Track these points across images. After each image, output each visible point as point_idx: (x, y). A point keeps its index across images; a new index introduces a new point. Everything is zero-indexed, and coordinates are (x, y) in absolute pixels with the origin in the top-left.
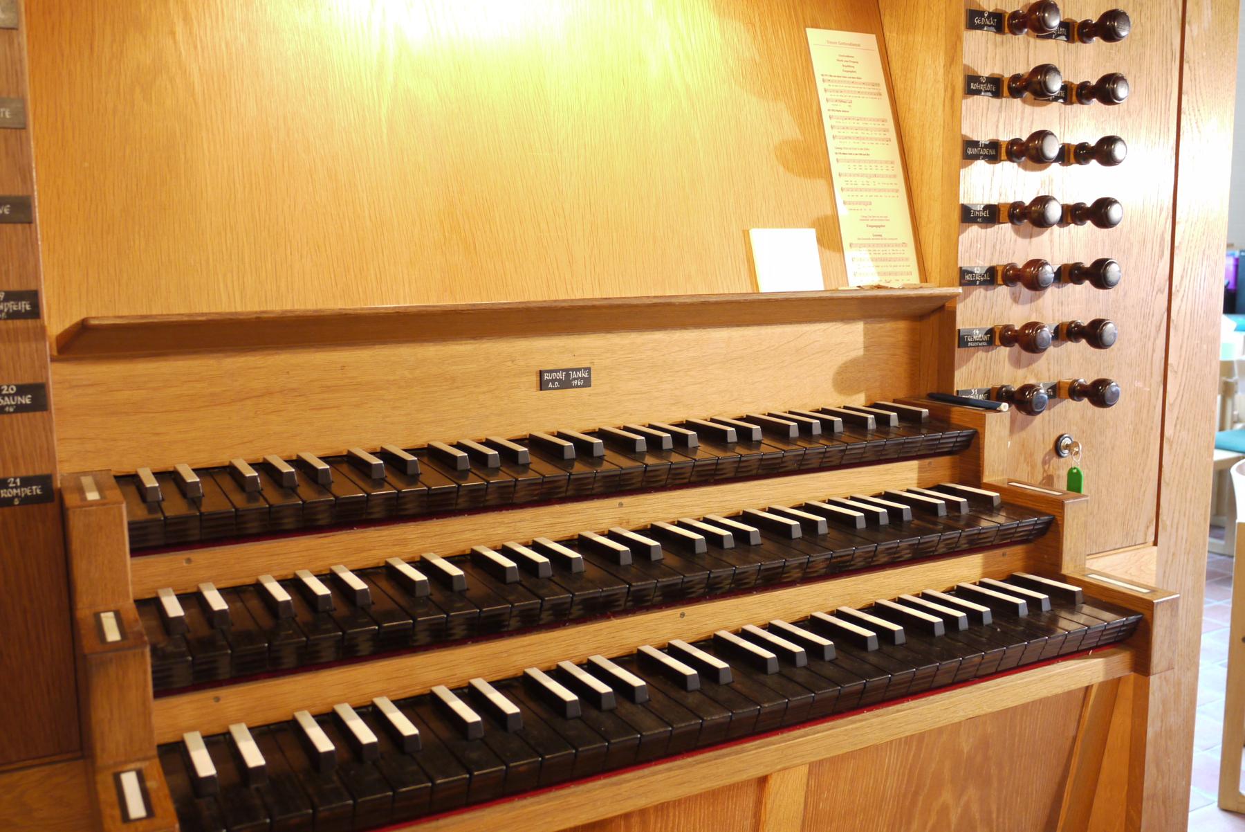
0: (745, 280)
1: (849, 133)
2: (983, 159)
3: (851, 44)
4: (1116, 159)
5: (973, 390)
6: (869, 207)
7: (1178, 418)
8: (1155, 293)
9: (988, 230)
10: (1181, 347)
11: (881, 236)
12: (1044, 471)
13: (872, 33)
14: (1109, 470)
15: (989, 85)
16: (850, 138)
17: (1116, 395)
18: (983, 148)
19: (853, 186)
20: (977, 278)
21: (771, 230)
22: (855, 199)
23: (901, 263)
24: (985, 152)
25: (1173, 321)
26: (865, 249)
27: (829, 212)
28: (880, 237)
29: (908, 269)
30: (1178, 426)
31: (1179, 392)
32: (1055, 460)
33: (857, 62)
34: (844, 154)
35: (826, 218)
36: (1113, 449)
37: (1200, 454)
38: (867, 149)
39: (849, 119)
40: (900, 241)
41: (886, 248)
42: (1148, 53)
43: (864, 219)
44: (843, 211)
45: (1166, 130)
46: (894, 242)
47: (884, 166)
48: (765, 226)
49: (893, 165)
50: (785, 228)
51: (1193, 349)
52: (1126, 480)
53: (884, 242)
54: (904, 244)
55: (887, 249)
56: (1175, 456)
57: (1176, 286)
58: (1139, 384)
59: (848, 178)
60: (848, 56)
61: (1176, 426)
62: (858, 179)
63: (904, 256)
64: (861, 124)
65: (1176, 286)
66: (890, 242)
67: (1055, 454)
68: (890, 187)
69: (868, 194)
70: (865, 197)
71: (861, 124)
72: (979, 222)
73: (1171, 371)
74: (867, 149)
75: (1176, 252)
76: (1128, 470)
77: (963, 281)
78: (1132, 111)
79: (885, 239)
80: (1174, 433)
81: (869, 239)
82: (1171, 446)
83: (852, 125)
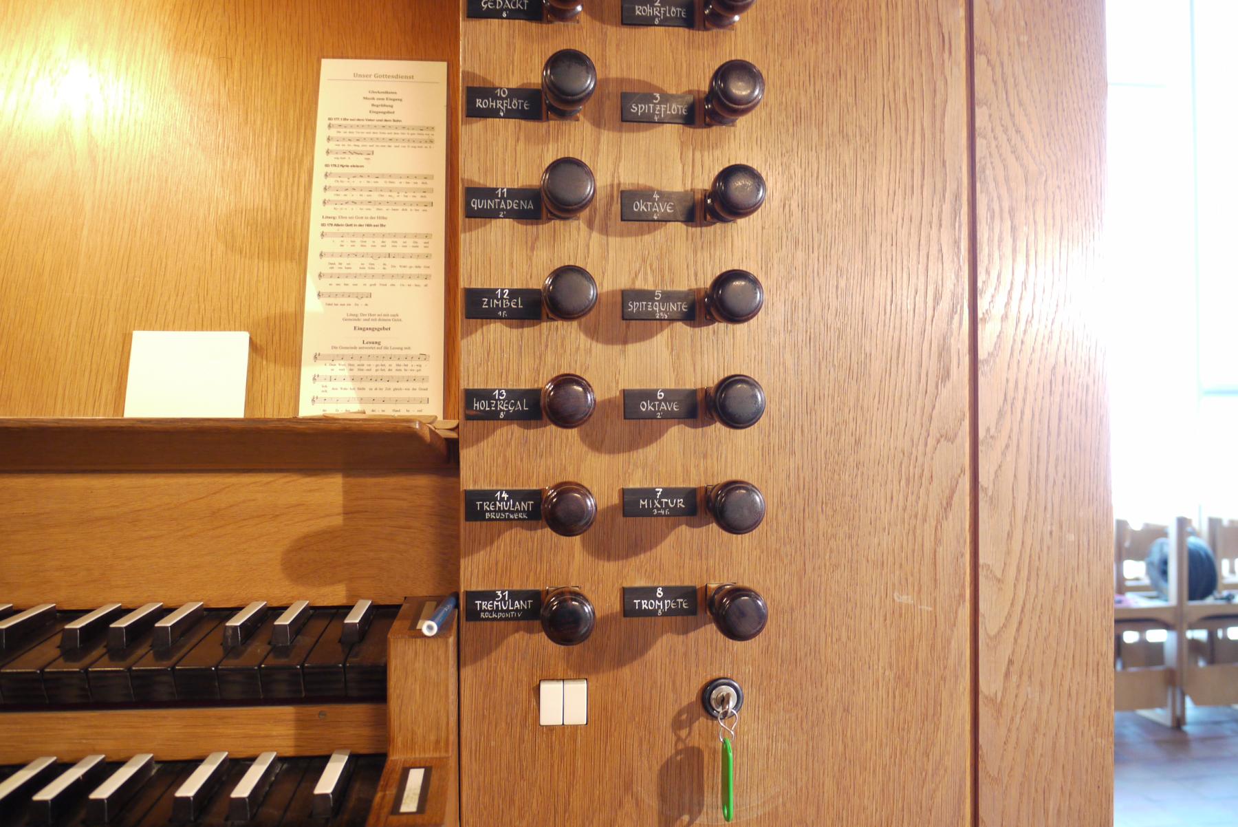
0: (106, 404)
1: (356, 196)
2: (505, 217)
3: (397, 77)
4: (538, 188)
5: (499, 593)
6: (365, 300)
7: (1011, 662)
8: (931, 442)
9: (526, 330)
10: (1010, 536)
11: (379, 343)
12: (679, 739)
13: (442, 60)
14: (841, 748)
15: (515, 101)
16: (354, 203)
17: (761, 618)
18: (508, 198)
19: (344, 271)
20: (500, 407)
21: (239, 332)
22: (334, 289)
23: (411, 385)
24: (512, 205)
25: (986, 490)
26: (342, 362)
27: (291, 308)
28: (377, 346)
29: (423, 394)
30: (1014, 678)
31: (1009, 616)
32: (702, 722)
33: (395, 93)
34: (338, 225)
35: (283, 316)
36: (846, 710)
37: (1076, 729)
38: (384, 218)
39: (361, 176)
40: (415, 352)
41: (384, 362)
42: (883, 39)
43: (354, 317)
44: (313, 304)
45: (938, 164)
46: (404, 352)
47: (410, 242)
48: (151, 327)
49: (426, 240)
50: (211, 330)
51: (1042, 539)
52: (884, 768)
53: (383, 352)
54: (423, 357)
55: (387, 363)
56: (1009, 730)
57: (988, 430)
58: (906, 599)
59: (332, 260)
60: (387, 93)
61: (1007, 675)
62: (352, 260)
63: (419, 374)
64: (381, 183)
65: (988, 430)
66: (398, 352)
67: (702, 711)
68: (415, 271)
69: (369, 281)
70: (361, 286)
71: (381, 183)
72: (501, 318)
73: (987, 577)
74: (384, 218)
75: (982, 369)
76: (888, 751)
77: (469, 412)
78: (850, 133)
79: (386, 348)
80: (1005, 689)
81: (355, 348)
82: (999, 712)
83: (363, 185)
